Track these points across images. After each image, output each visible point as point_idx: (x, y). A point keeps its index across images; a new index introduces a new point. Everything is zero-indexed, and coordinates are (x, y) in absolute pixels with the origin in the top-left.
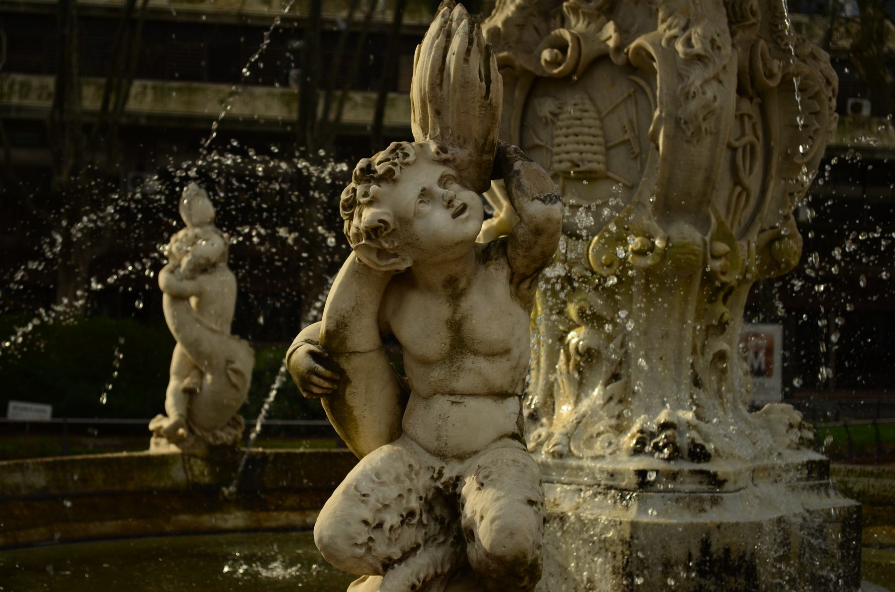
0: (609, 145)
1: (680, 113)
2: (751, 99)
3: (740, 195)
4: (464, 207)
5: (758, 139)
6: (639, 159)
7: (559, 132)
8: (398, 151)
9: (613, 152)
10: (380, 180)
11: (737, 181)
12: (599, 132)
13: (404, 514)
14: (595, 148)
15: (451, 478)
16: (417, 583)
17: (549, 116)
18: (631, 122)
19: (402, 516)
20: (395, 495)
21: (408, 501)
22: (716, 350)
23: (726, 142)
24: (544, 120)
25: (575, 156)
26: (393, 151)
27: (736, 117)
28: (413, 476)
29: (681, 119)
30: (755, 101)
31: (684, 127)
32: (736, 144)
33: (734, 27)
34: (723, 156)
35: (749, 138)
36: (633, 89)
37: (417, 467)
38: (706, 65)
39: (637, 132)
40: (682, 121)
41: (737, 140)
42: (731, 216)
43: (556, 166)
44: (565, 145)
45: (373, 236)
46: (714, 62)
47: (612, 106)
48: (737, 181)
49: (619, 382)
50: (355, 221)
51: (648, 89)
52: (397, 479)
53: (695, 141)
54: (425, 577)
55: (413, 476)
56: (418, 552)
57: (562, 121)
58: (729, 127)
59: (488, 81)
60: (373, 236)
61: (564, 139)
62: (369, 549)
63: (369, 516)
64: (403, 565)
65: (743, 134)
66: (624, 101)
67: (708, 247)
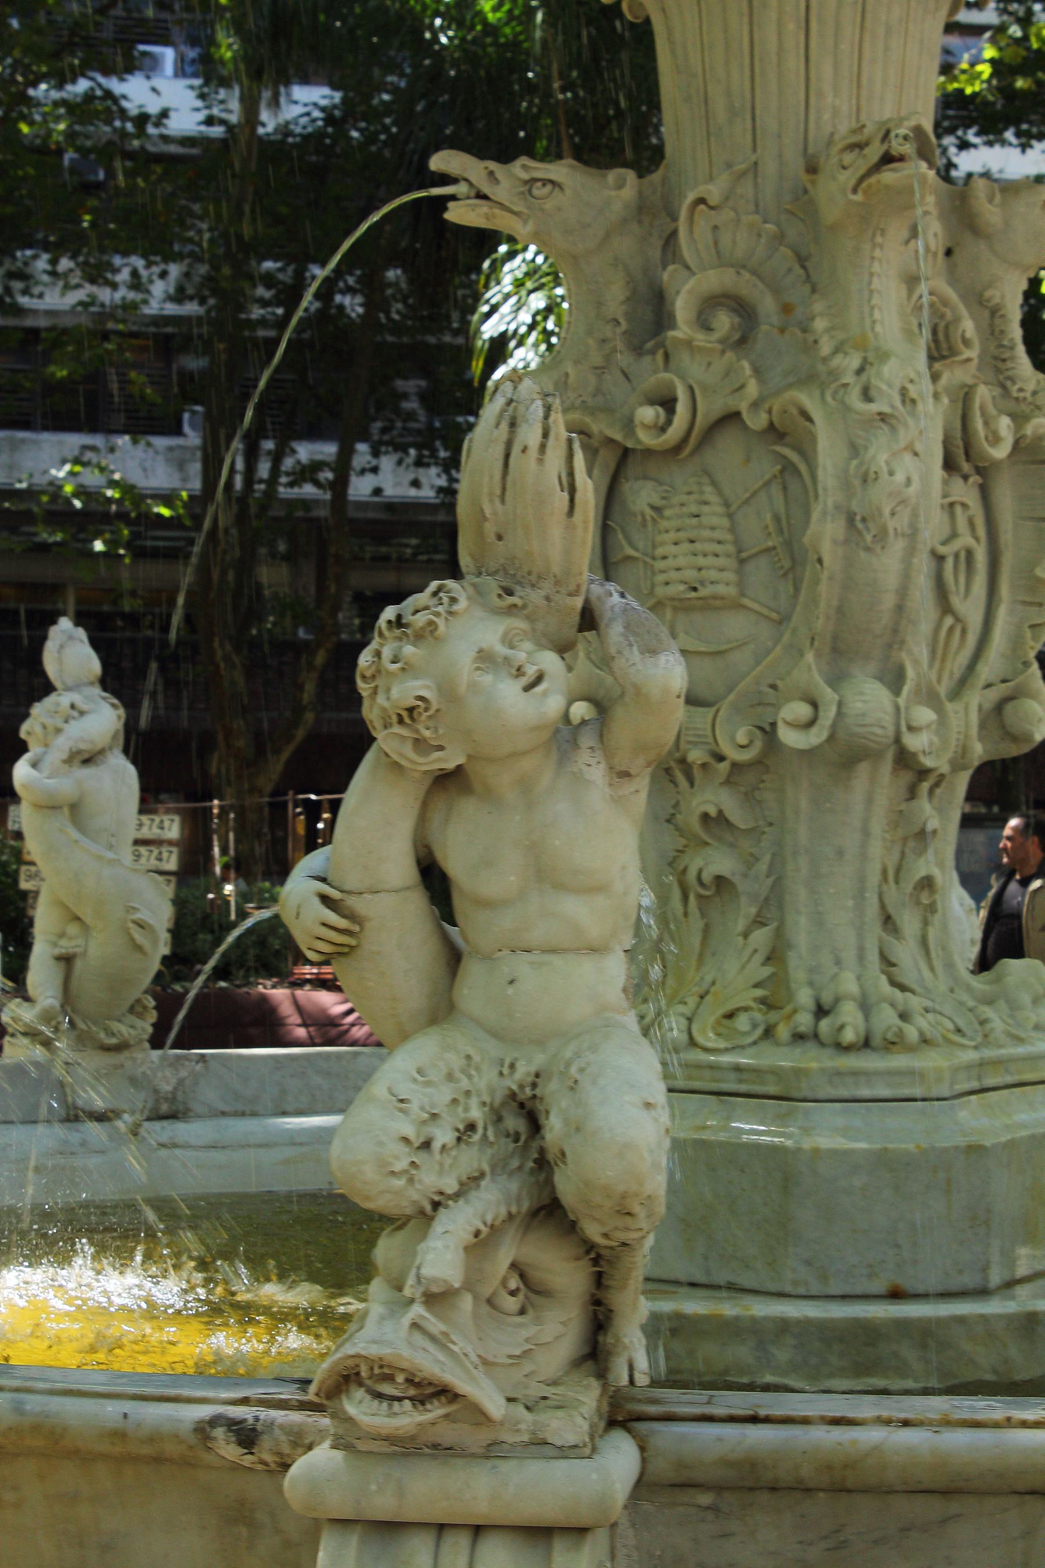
0: (744, 555)
1: (854, 506)
2: (965, 478)
3: (951, 629)
4: (539, 679)
5: (977, 539)
6: (790, 576)
7: (666, 537)
8: (441, 594)
9: (750, 567)
10: (419, 637)
11: (945, 606)
12: (729, 537)
13: (461, 1127)
14: (721, 561)
15: (528, 1074)
16: (482, 1227)
17: (649, 512)
18: (777, 519)
19: (458, 1130)
20: (447, 1098)
21: (466, 1110)
22: (922, 873)
23: (929, 548)
24: (639, 518)
25: (690, 574)
26: (435, 594)
27: (942, 507)
28: (473, 1072)
29: (855, 514)
30: (971, 480)
31: (860, 526)
32: (942, 550)
33: (937, 366)
34: (923, 565)
35: (966, 540)
36: (779, 467)
37: (477, 1058)
38: (893, 429)
39: (786, 534)
40: (858, 518)
41: (944, 543)
42: (937, 664)
43: (660, 591)
44: (675, 557)
45: (407, 720)
46: (906, 425)
47: (747, 495)
48: (945, 606)
49: (765, 929)
50: (381, 699)
51: (803, 468)
52: (450, 1077)
53: (878, 550)
54: (494, 1220)
55: (473, 1072)
56: (483, 1183)
57: (668, 519)
58: (933, 527)
59: (572, 491)
60: (407, 720)
61: (673, 549)
62: (411, 1180)
63: (409, 1131)
64: (461, 1202)
65: (954, 535)
66: (767, 484)
67: (903, 716)
